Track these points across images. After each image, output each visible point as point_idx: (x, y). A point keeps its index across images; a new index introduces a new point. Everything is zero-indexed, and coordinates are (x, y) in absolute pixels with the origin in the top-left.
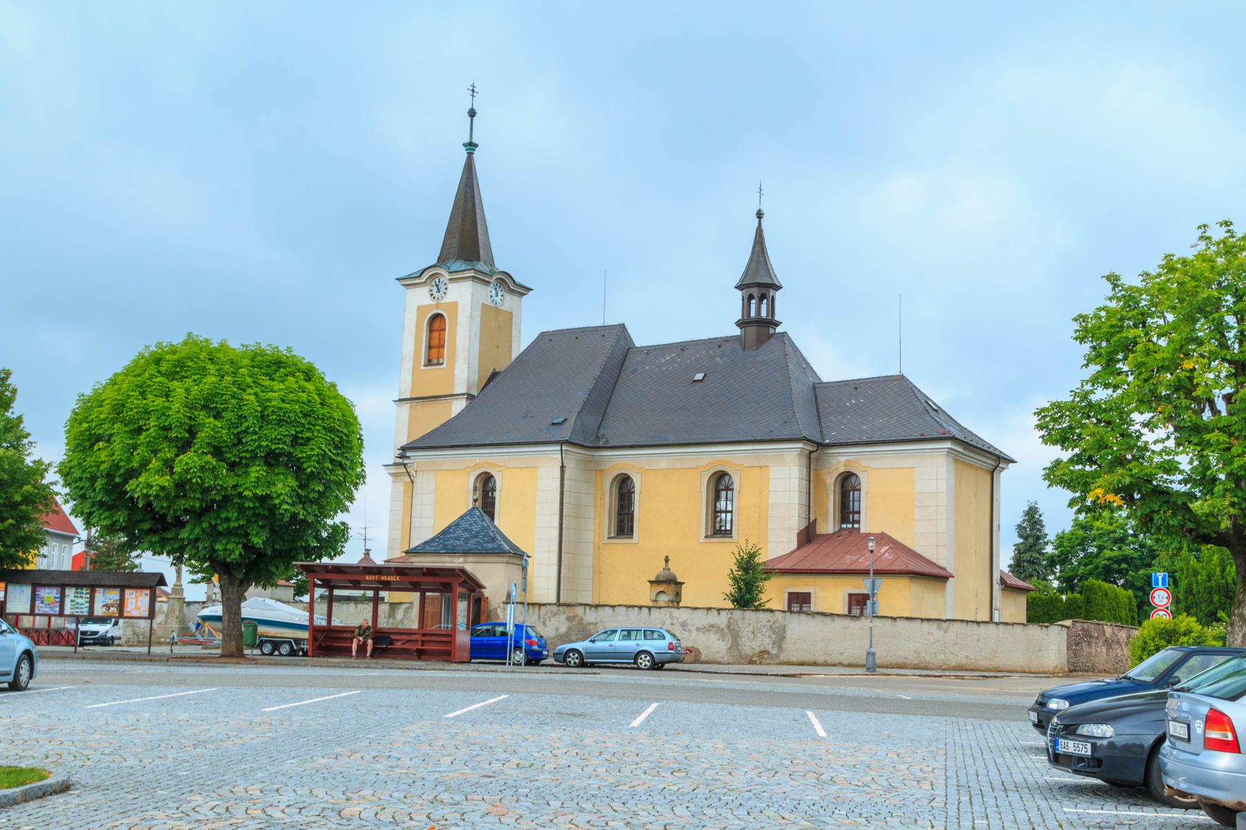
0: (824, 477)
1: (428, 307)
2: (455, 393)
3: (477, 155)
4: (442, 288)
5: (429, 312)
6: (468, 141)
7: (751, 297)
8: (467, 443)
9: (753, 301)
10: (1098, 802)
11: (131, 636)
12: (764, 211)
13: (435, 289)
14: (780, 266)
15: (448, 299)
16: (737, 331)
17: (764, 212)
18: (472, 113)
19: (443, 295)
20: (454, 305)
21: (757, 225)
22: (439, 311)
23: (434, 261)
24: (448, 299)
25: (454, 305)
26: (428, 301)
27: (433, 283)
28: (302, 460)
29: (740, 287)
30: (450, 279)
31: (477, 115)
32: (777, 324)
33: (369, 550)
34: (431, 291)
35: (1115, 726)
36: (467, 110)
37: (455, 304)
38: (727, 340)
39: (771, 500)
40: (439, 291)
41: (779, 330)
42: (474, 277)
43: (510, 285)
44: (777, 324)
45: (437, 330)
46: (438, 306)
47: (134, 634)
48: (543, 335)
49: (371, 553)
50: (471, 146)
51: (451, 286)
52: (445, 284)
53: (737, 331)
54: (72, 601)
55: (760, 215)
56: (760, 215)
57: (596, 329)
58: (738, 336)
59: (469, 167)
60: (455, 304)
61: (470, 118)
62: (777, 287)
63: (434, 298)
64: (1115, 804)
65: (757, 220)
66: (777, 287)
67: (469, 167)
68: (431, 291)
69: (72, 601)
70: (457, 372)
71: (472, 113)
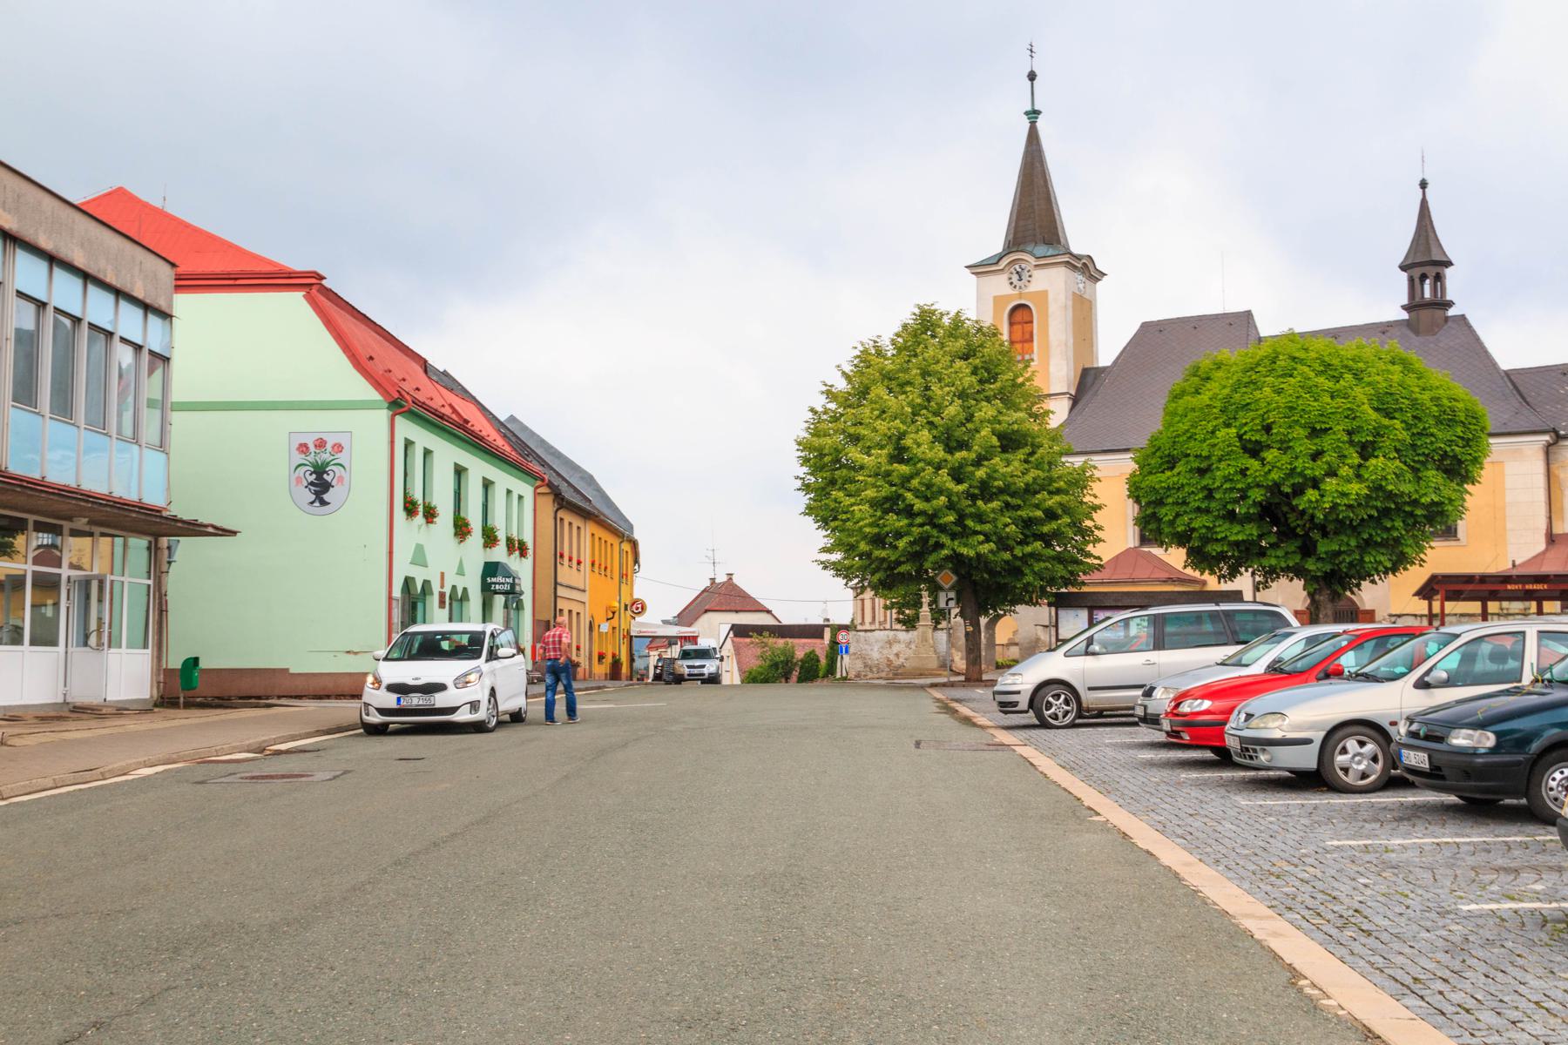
0: (1557, 472)
1: (1009, 297)
2: (1052, 392)
3: (1041, 123)
4: (1025, 276)
5: (1035, 304)
6: (1029, 108)
7: (1423, 277)
8: (1124, 447)
9: (1428, 281)
10: (1451, 827)
11: (862, 670)
12: (1429, 180)
13: (1015, 278)
14: (1450, 239)
15: (1033, 288)
16: (1405, 315)
17: (1428, 181)
18: (1032, 77)
19: (1027, 284)
20: (1043, 295)
21: (1421, 197)
22: (1023, 302)
23: (998, 247)
24: (1033, 288)
25: (1043, 295)
26: (1007, 290)
27: (1012, 269)
28: (1466, 463)
29: (1403, 268)
30: (1036, 266)
31: (1037, 78)
32: (1450, 304)
33: (732, 574)
34: (1010, 279)
35: (1222, 744)
36: (1027, 74)
37: (1044, 294)
38: (1390, 325)
39: (1508, 499)
40: (1020, 280)
41: (1451, 312)
42: (1068, 262)
43: (1087, 269)
44: (1450, 304)
45: (1019, 323)
46: (1020, 296)
47: (866, 666)
48: (1146, 326)
49: (734, 577)
50: (1033, 114)
51: (1037, 274)
52: (1029, 271)
53: (1405, 315)
54: (1138, 625)
55: (1423, 185)
56: (1423, 185)
57: (1216, 316)
58: (28, 331)
59: (1033, 138)
60: (1044, 294)
61: (1030, 82)
62: (1448, 264)
63: (1015, 287)
64: (1471, 824)
65: (1421, 190)
66: (1448, 264)
67: (1033, 138)
68: (1010, 279)
69: (1138, 625)
70: (1052, 369)
71: (1032, 77)
